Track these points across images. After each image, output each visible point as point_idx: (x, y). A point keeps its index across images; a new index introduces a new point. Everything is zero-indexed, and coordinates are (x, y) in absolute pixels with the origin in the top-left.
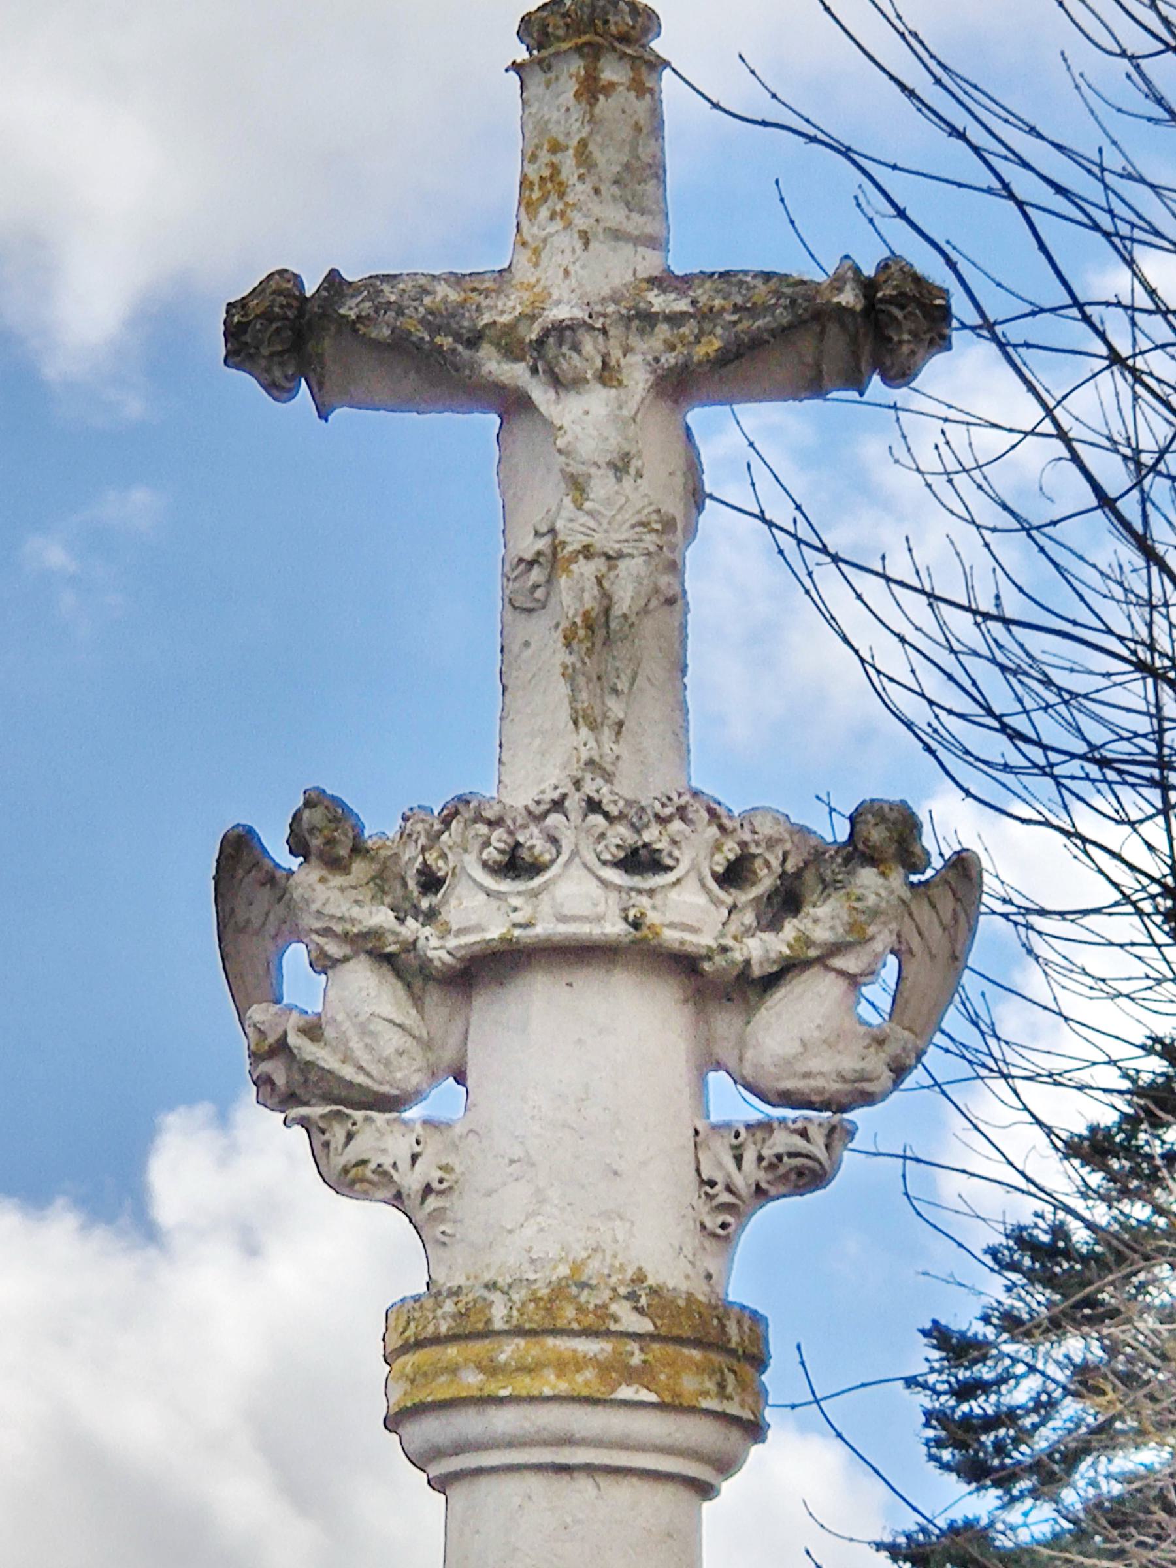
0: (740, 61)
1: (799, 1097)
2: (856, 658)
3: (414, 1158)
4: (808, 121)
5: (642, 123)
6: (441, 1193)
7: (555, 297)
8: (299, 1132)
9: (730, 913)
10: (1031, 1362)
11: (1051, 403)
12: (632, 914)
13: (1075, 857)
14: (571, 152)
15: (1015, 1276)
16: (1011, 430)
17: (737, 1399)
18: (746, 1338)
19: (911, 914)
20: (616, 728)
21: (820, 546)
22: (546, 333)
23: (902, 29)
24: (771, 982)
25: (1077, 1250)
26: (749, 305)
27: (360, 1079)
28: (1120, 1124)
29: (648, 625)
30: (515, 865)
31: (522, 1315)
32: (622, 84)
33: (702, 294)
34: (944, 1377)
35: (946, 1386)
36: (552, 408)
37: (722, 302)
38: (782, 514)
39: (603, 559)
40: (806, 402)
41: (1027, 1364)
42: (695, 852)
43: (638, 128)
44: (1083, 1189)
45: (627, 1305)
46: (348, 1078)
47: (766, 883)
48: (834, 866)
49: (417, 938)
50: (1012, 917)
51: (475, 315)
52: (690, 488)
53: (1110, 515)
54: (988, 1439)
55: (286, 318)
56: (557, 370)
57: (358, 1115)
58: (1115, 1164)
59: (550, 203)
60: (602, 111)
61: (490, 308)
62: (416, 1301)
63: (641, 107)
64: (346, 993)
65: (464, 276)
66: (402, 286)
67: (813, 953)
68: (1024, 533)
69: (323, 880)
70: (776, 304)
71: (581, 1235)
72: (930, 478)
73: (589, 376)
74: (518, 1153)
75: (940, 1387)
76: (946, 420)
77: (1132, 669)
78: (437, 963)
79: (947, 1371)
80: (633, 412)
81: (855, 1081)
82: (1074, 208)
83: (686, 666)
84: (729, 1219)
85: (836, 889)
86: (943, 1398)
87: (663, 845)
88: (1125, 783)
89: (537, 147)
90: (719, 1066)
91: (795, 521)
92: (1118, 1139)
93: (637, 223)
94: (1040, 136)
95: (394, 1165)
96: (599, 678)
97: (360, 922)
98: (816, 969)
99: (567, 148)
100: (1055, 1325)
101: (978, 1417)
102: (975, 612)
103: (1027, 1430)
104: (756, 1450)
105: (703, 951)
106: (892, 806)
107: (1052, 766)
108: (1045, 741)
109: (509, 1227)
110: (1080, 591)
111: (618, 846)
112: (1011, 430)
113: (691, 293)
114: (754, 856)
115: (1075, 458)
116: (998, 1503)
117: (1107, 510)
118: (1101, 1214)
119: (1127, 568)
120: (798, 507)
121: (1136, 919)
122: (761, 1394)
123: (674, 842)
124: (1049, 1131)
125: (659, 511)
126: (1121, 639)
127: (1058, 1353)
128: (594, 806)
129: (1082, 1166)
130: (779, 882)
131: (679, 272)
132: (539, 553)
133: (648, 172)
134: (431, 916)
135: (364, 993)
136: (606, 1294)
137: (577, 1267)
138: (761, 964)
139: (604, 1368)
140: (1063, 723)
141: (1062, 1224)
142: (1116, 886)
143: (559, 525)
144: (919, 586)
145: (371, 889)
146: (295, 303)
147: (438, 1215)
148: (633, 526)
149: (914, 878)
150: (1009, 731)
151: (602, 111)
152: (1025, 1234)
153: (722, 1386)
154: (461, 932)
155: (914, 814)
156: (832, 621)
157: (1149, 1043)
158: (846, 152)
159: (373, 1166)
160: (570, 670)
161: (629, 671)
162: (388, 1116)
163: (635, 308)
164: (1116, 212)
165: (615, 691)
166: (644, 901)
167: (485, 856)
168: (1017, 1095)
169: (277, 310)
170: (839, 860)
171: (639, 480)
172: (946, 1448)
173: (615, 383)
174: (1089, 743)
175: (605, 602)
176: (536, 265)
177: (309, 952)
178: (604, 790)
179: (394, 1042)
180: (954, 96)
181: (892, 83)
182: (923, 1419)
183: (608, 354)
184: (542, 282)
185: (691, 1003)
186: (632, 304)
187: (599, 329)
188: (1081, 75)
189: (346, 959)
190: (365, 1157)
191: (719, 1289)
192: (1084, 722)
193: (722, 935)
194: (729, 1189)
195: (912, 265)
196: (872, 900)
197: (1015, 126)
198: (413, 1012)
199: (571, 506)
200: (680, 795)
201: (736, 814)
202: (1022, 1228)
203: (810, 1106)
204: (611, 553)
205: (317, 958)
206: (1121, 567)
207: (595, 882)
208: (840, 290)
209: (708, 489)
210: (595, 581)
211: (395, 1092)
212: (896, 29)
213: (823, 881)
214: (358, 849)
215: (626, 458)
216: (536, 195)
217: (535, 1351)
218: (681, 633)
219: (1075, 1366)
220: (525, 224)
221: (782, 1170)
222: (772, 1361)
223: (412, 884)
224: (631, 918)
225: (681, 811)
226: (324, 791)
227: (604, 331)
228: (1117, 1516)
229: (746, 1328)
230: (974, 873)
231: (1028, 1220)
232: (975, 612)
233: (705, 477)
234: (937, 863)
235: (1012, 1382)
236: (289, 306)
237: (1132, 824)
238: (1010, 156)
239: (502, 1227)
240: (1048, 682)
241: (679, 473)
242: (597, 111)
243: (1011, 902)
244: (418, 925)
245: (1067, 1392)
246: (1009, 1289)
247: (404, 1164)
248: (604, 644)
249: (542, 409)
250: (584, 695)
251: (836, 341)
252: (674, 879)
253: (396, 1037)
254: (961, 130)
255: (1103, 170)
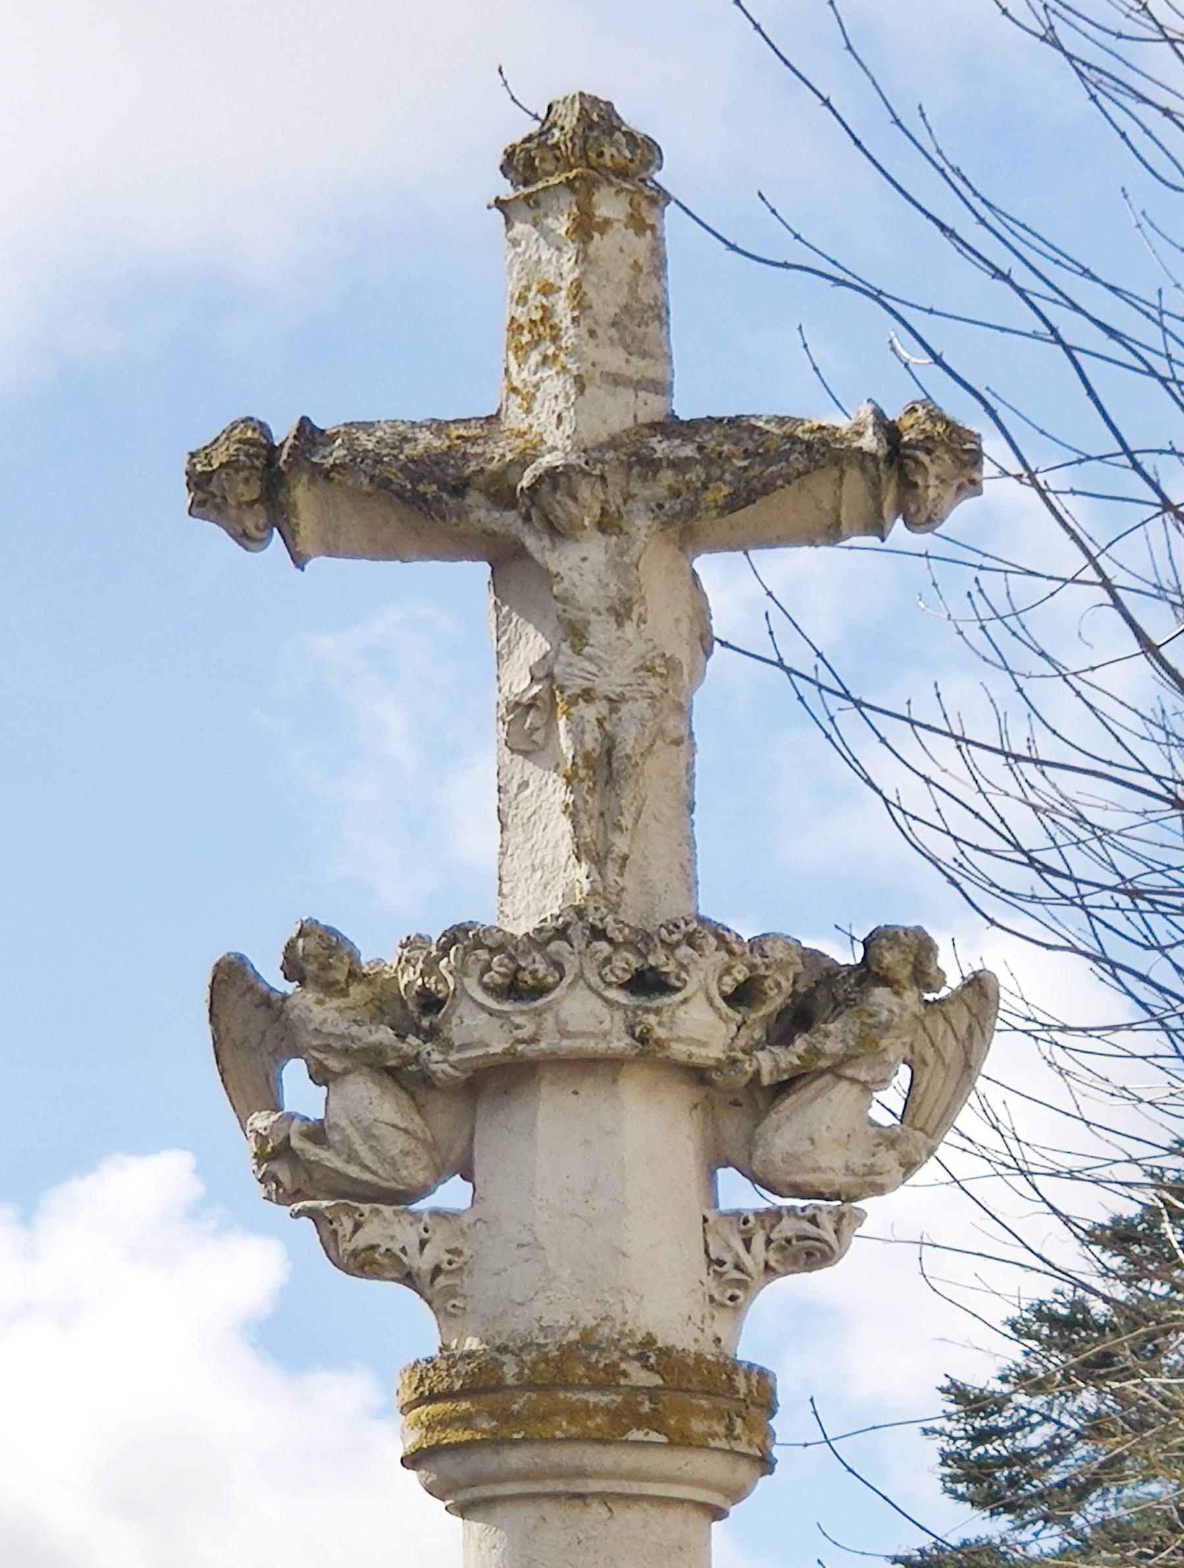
0: (759, 199)
1: (809, 1188)
2: (880, 798)
3: (423, 1244)
4: (834, 262)
5: (641, 262)
6: (448, 1273)
7: (550, 443)
8: (306, 1223)
9: (739, 1028)
10: (1047, 1413)
11: (1095, 551)
12: (638, 1030)
13: (1101, 979)
14: (563, 293)
15: (1033, 1344)
16: (1050, 578)
17: (744, 1439)
18: (754, 1390)
19: (925, 1029)
20: (620, 861)
21: (842, 691)
22: (539, 480)
23: (942, 164)
24: (782, 1089)
25: (1095, 1321)
26: (761, 451)
27: (366, 1176)
28: (1142, 1216)
29: (652, 765)
30: (514, 989)
31: (533, 1373)
32: (618, 220)
33: (709, 440)
34: (961, 1426)
35: (962, 1433)
36: (547, 554)
37: (733, 447)
38: (802, 659)
39: (605, 702)
40: (822, 549)
41: (1041, 1414)
42: (704, 975)
43: (636, 266)
44: (1104, 1271)
45: (637, 1364)
46: (354, 1176)
47: (776, 1001)
48: (846, 987)
49: (418, 1053)
50: (1033, 1033)
51: (460, 463)
52: (697, 634)
53: (1154, 662)
54: (1002, 1475)
55: (253, 467)
56: (551, 517)
57: (366, 1208)
58: (1136, 1249)
59: (542, 348)
60: (597, 249)
61: (477, 455)
62: (428, 1362)
63: (640, 246)
64: (348, 1102)
65: (447, 422)
66: (379, 433)
67: (823, 1063)
68: (1061, 678)
69: (320, 1002)
70: (790, 449)
71: (589, 1307)
72: (961, 626)
73: (586, 523)
74: (526, 1237)
75: (955, 1434)
76: (981, 568)
77: (1169, 806)
78: (440, 1075)
79: (963, 1421)
80: (635, 559)
81: (864, 1175)
82: (1129, 354)
83: (694, 803)
84: (738, 1292)
85: (847, 1006)
86: (959, 1443)
87: (671, 968)
88: (1157, 911)
89: (528, 288)
90: (727, 1164)
91: (816, 668)
92: (1140, 1228)
93: (638, 367)
94: (1094, 278)
95: (403, 1250)
96: (602, 815)
97: (360, 1039)
98: (828, 1078)
99: (560, 289)
100: (1067, 1384)
101: (992, 1457)
102: (1007, 755)
103: (1040, 1468)
104: (764, 1481)
105: (713, 1063)
106: (906, 931)
107: (1082, 897)
108: (1077, 875)
109: (519, 1300)
110: (1117, 733)
111: (624, 970)
112: (1050, 578)
113: (698, 439)
114: (765, 977)
115: (1117, 603)
116: (1011, 1526)
117: (1149, 655)
118: (1120, 1292)
119: (1169, 712)
120: (819, 655)
121: (1163, 1034)
122: (770, 1434)
123: (683, 967)
124: (1067, 1221)
125: (664, 655)
126: (1158, 778)
127: (1073, 1406)
128: (598, 933)
129: (1103, 1251)
130: (790, 1001)
131: (684, 416)
132: (535, 697)
133: (650, 314)
134: (431, 1034)
135: (366, 1102)
136: (616, 1356)
137: (587, 1334)
138: (771, 1073)
139: (614, 1414)
140: (1098, 859)
141: (1082, 1300)
142: (1144, 1006)
143: (557, 670)
144: (947, 729)
145: (369, 1010)
146: (264, 452)
147: (451, 1292)
148: (635, 670)
149: (929, 997)
150: (1037, 865)
151: (597, 249)
152: (1044, 1308)
153: (730, 1428)
154: (462, 1047)
155: (930, 938)
156: (855, 765)
157: (1176, 1146)
158: (877, 296)
159: (382, 1250)
160: (571, 808)
161: (633, 809)
162: (395, 1208)
163: (635, 454)
164: (1173, 357)
165: (619, 827)
166: (652, 1019)
167: (486, 979)
168: (1036, 1189)
169: (242, 458)
170: (852, 981)
171: (642, 626)
172: (961, 1482)
173: (616, 530)
174: (1122, 877)
175: (607, 743)
176: (528, 411)
177: (308, 1066)
178: (609, 919)
179: (399, 1144)
180: (998, 235)
181: (930, 222)
182: (940, 1460)
183: (607, 502)
184: (534, 429)
185: (698, 1111)
186: (632, 450)
187: (596, 476)
188: (1143, 213)
189: (346, 1072)
190: (373, 1242)
191: (726, 1351)
192: (1117, 856)
193: (732, 1049)
194: (738, 1267)
195: (940, 409)
196: (884, 1016)
197: (1065, 266)
198: (417, 1119)
199: (569, 651)
200: (687, 924)
201: (746, 940)
202: (1042, 1302)
203: (820, 1196)
204: (613, 697)
205: (317, 1072)
206: (1163, 712)
207: (600, 1002)
208: (860, 434)
209: (716, 634)
210: (595, 723)
211: (402, 1187)
212: (934, 163)
213: (834, 998)
214: (354, 975)
215: (628, 603)
216: (526, 338)
217: (546, 1403)
218: (687, 772)
219: (1089, 1415)
220: (514, 368)
221: (790, 1250)
222: (779, 1409)
223: (411, 1006)
224: (637, 1034)
225: (690, 940)
226: (317, 922)
227: (603, 478)
228: (1115, 1534)
229: (754, 1382)
230: (991, 994)
231: (1048, 1296)
232: (1007, 755)
233: (713, 622)
234: (954, 980)
235: (1027, 1429)
236: (257, 456)
237: (1161, 949)
238: (1060, 299)
239: (513, 1301)
240: (1080, 819)
241: (685, 620)
242: (591, 248)
243: (1035, 1021)
244: (418, 1042)
245: (1079, 1436)
246: (1026, 1354)
247: (413, 1250)
248: (607, 783)
249: (537, 556)
250: (587, 831)
251: (855, 482)
252: (681, 998)
253: (400, 1141)
254: (1006, 272)
255: (1162, 313)
